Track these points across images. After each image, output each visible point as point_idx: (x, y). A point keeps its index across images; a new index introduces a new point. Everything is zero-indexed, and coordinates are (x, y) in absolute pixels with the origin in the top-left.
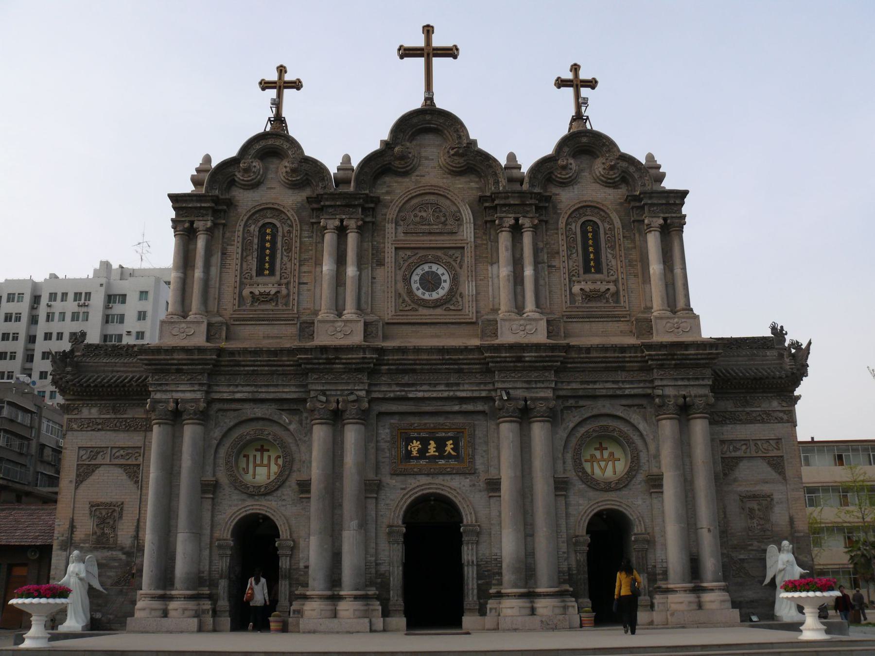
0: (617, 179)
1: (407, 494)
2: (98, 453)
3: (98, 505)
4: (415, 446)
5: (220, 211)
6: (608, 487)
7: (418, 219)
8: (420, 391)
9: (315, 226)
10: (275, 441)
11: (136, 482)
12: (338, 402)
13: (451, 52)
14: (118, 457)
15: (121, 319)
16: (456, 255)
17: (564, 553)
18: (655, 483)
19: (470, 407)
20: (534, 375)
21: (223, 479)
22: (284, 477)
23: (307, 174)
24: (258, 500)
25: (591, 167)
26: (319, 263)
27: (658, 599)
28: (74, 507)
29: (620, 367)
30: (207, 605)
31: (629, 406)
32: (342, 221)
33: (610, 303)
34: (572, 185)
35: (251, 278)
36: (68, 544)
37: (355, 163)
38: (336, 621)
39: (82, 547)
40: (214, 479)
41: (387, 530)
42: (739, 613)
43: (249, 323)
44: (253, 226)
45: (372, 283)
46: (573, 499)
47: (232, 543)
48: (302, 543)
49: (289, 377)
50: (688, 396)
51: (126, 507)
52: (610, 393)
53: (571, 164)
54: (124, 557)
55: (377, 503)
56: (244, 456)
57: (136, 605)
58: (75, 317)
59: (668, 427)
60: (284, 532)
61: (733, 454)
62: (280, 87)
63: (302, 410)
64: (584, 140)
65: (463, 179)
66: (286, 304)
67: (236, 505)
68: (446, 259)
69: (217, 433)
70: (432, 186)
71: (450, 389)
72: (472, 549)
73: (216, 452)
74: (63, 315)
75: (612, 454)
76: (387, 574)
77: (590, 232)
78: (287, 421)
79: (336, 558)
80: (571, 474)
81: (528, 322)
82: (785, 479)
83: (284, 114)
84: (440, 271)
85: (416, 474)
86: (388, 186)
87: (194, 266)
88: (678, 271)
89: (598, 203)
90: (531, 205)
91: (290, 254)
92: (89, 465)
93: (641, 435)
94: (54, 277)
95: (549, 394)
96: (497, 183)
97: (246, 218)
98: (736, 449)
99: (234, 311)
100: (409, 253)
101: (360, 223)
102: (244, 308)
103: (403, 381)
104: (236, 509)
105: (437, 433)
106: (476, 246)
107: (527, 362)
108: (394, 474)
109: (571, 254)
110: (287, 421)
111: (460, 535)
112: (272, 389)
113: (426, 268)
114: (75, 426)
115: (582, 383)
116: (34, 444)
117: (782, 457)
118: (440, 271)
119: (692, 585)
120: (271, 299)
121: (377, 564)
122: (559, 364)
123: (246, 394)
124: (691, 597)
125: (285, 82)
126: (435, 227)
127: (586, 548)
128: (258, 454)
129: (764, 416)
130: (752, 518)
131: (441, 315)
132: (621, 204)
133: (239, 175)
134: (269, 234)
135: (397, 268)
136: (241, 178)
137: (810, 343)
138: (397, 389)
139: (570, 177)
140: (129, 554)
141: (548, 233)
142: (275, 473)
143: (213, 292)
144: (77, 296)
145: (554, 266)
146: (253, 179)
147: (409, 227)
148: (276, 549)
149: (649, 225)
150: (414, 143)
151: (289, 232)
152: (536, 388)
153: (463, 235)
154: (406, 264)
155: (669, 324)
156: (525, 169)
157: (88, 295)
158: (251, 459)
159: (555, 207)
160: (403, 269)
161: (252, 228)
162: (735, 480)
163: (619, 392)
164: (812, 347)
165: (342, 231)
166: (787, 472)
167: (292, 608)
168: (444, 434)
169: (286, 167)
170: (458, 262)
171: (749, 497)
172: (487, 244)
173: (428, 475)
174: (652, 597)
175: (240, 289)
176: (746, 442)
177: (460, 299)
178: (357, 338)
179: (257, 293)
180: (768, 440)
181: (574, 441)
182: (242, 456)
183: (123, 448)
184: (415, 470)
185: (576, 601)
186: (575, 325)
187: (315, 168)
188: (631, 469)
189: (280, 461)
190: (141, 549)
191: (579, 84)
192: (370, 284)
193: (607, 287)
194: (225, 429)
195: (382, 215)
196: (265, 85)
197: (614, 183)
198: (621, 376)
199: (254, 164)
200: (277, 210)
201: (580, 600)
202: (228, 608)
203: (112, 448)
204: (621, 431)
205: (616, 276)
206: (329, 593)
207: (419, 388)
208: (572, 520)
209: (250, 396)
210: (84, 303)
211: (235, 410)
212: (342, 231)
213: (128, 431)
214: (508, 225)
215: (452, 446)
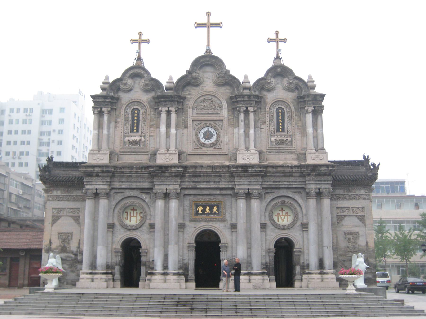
0: (293, 88)
1: (196, 230)
2: (61, 211)
3: (62, 234)
4: (200, 209)
5: (114, 103)
6: (284, 228)
7: (202, 107)
8: (203, 185)
9: (156, 110)
10: (139, 206)
11: (78, 223)
12: (167, 190)
13: (218, 25)
14: (70, 212)
15: (50, 123)
16: (220, 123)
17: (264, 256)
18: (305, 226)
19: (224, 192)
20: (252, 179)
21: (117, 223)
22: (143, 222)
23: (153, 86)
24: (132, 232)
25: (282, 82)
26: (158, 127)
27: (304, 277)
28: (51, 235)
29: (291, 175)
30: (110, 276)
31: (295, 192)
32: (169, 108)
33: (288, 146)
34: (273, 91)
35: (128, 133)
36: (49, 250)
37: (175, 80)
38: (165, 283)
39: (55, 252)
40: (113, 223)
41: (188, 245)
42: (339, 284)
43: (127, 154)
44: (129, 110)
45: (182, 136)
46: (268, 232)
47: (121, 250)
48: (151, 251)
49: (146, 178)
50: (321, 189)
51: (73, 234)
52: (286, 186)
53: (272, 81)
54: (73, 256)
55: (183, 234)
56: (126, 212)
57: (79, 276)
58: (25, 122)
59: (312, 202)
60: (143, 246)
61: (342, 214)
62: (140, 43)
63: (151, 193)
64: (279, 70)
65: (223, 88)
66: (144, 145)
67: (123, 234)
68: (215, 125)
69: (114, 203)
70: (209, 91)
71: (216, 184)
72: (224, 254)
73: (114, 211)
74: (18, 121)
75: (287, 213)
76: (187, 264)
77: (280, 113)
78: (145, 197)
79: (166, 257)
80: (268, 222)
81: (250, 155)
82: (365, 225)
83: (142, 56)
84: (212, 130)
85: (200, 221)
86: (190, 91)
87: (103, 128)
88: (319, 131)
89: (284, 99)
90: (253, 101)
91: (145, 123)
92: (57, 216)
93: (300, 205)
94: (12, 100)
95: (259, 187)
96: (238, 90)
97: (125, 106)
98: (343, 212)
99: (121, 148)
100: (198, 122)
101: (177, 109)
102: (125, 147)
103: (195, 181)
104: (122, 235)
105: (210, 203)
106: (228, 119)
107: (250, 173)
108: (191, 221)
109: (271, 123)
110: (145, 197)
111: (219, 248)
112: (138, 184)
113: (206, 129)
114: (50, 199)
115: (274, 182)
116: (6, 193)
117: (364, 215)
118: (212, 130)
119: (319, 271)
120: (137, 143)
121: (183, 260)
122: (263, 173)
123: (127, 186)
124: (319, 276)
125: (142, 40)
126: (210, 110)
127: (273, 254)
128: (132, 212)
129: (357, 197)
130: (349, 242)
131: (212, 151)
132: (294, 100)
133: (122, 86)
134: (136, 113)
135: (193, 129)
136: (123, 87)
137: (379, 164)
138: (193, 184)
139: (272, 87)
140: (76, 255)
141: (261, 113)
142: (140, 220)
143: (111, 140)
144: (25, 110)
145: (263, 129)
146: (128, 88)
147: (199, 110)
148: (140, 253)
149: (307, 111)
150: (201, 71)
151: (145, 112)
152: (253, 184)
153: (223, 114)
154: (197, 127)
155: (313, 156)
156: (252, 83)
157: (32, 110)
158: (129, 213)
159: (265, 102)
160: (196, 130)
161: (128, 111)
162: (342, 225)
163: (290, 186)
164: (380, 166)
165: (169, 113)
166: (366, 222)
167: (147, 278)
168: (213, 204)
169: (143, 82)
170: (220, 127)
171: (348, 233)
172: (233, 118)
173: (206, 221)
174: (302, 276)
175: (123, 139)
176: (348, 208)
177: (221, 144)
178: (175, 161)
179: (131, 140)
180: (358, 208)
181: (270, 207)
182: (125, 212)
183: (72, 209)
184: (200, 219)
185: (269, 277)
186: (272, 156)
187: (156, 84)
188: (294, 220)
189: (142, 215)
190: (81, 253)
191: (278, 41)
192: (181, 137)
193: (287, 138)
194: (117, 201)
195: (187, 105)
196: (133, 41)
197: (292, 90)
198: (291, 179)
199: (129, 81)
200: (140, 102)
201: (270, 277)
202: (119, 278)
203: (67, 208)
204: (291, 203)
205: (291, 133)
206: (163, 272)
207: (202, 184)
208: (268, 242)
209: (129, 187)
210: (29, 114)
211: (122, 193)
212: (169, 113)
213: (74, 201)
214: (243, 110)
215: (216, 209)
